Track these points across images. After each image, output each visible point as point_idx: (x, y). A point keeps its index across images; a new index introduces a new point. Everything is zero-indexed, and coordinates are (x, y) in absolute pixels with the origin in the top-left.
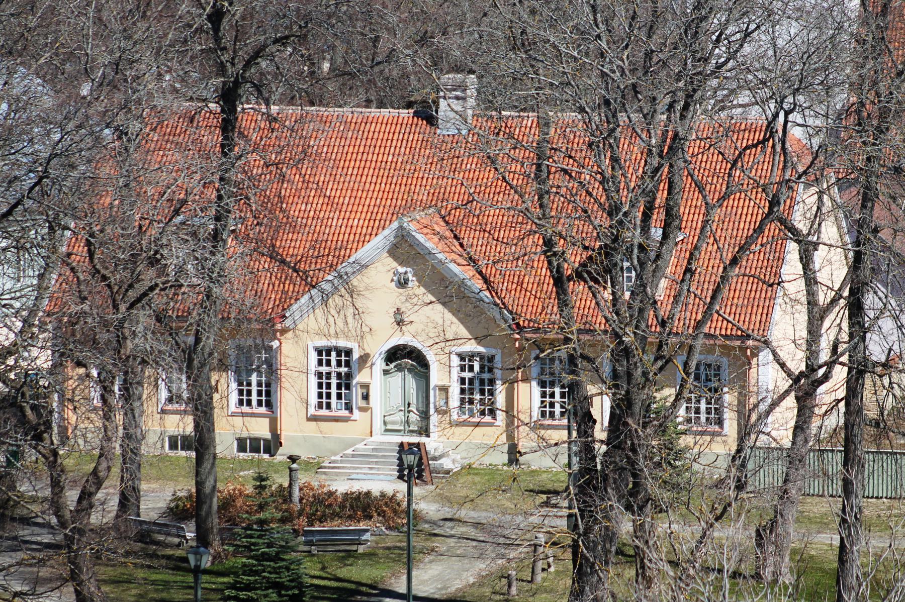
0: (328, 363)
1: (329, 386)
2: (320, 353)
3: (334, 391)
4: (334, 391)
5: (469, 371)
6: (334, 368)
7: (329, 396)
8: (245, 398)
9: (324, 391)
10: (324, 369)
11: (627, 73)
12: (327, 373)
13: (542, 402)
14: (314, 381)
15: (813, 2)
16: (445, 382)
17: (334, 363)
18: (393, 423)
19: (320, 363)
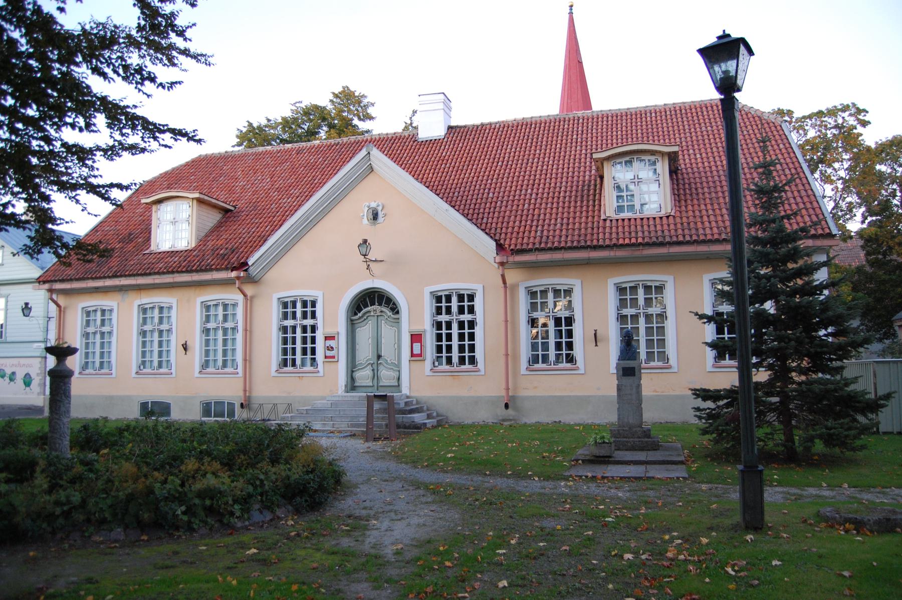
1: (449, 337)
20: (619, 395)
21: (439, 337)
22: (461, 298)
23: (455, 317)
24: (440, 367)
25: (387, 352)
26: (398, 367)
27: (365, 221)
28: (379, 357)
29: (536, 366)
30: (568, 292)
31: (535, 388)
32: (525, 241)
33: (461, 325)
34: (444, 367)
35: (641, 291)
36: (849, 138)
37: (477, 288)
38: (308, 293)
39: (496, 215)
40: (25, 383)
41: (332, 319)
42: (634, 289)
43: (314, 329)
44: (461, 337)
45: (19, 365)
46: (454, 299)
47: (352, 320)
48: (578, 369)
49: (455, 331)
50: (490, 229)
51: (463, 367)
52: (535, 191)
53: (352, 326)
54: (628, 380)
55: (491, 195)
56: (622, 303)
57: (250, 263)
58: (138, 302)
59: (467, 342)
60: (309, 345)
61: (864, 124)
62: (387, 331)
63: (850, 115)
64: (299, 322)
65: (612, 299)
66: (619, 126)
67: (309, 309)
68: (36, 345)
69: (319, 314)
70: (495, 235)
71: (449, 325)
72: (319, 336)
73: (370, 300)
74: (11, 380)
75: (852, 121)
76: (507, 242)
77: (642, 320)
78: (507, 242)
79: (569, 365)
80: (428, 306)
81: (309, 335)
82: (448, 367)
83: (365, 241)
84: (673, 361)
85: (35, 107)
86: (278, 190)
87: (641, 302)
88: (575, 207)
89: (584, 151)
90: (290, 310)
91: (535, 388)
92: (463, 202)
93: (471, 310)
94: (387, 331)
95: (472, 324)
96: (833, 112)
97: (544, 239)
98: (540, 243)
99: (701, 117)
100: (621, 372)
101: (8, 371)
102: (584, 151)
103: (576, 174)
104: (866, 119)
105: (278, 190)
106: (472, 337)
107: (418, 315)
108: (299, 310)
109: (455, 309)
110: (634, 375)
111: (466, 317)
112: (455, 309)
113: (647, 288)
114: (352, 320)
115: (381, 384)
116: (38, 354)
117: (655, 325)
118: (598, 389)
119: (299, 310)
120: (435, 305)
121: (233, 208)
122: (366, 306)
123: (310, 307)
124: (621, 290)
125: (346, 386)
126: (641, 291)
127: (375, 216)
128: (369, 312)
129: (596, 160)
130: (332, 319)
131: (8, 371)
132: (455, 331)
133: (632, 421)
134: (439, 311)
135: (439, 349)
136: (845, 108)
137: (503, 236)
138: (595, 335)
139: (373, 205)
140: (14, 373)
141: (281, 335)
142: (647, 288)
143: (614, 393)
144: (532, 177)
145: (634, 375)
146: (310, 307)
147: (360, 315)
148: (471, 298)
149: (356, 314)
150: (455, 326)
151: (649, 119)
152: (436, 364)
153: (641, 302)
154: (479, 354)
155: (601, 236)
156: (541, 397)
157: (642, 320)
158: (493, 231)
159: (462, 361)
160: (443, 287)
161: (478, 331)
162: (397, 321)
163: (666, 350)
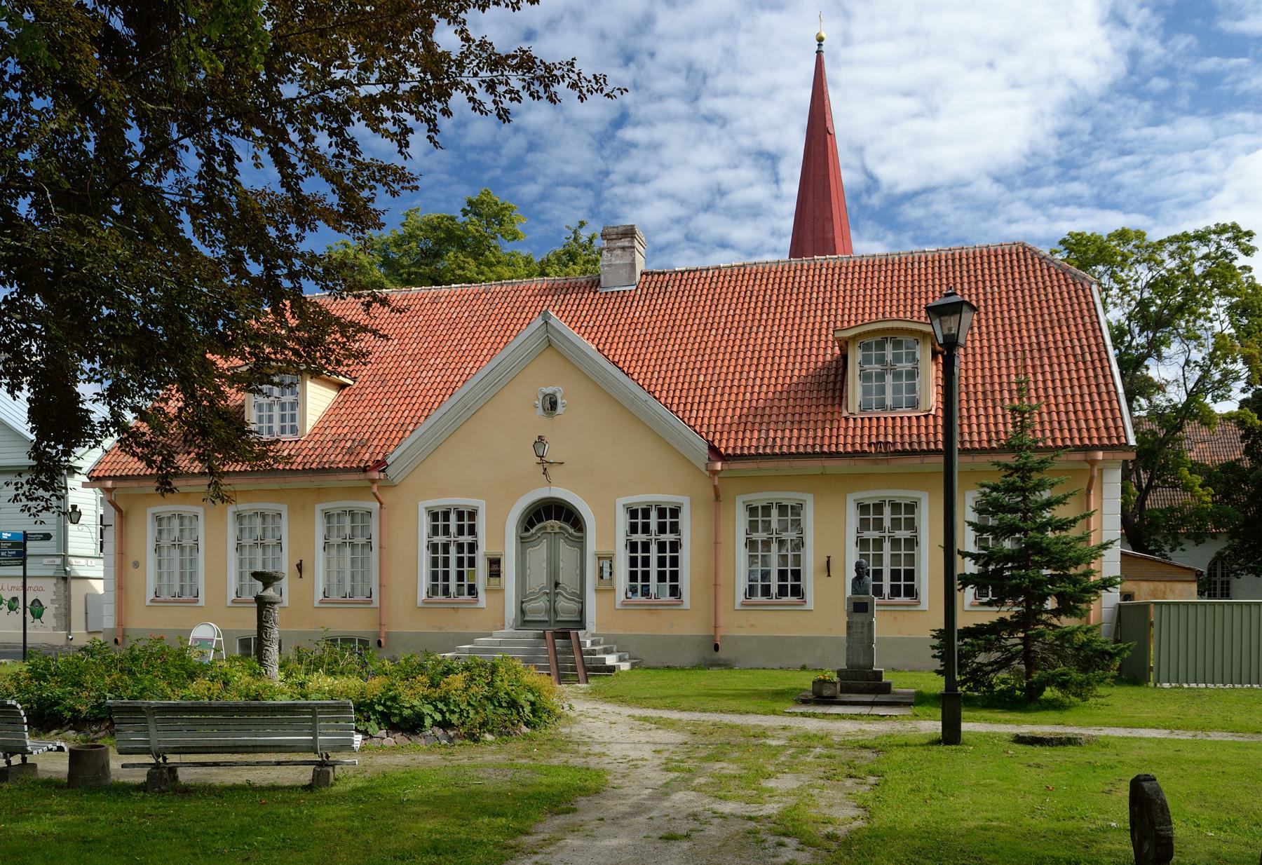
0: (446, 531)
1: (646, 562)
2: (435, 516)
3: (654, 569)
4: (654, 569)
5: (643, 532)
6: (453, 537)
7: (646, 576)
8: (440, 583)
9: (640, 569)
10: (640, 537)
11: (1210, 64)
12: (643, 543)
13: (751, 572)
14: (425, 556)
15: (3, 356)
16: (606, 549)
17: (453, 529)
18: (534, 611)
19: (435, 531)
20: (849, 634)
21: (633, 562)
22: (662, 513)
24: (634, 599)
25: (567, 578)
26: (581, 597)
27: (540, 411)
28: (557, 585)
30: (911, 508)
31: (752, 626)
32: (747, 443)
34: (440, 598)
35: (887, 510)
36: (1222, 274)
37: (684, 501)
38: (465, 502)
39: (709, 406)
42: (879, 507)
43: (473, 547)
44: (662, 561)
46: (654, 514)
49: (654, 554)
50: (701, 426)
51: (897, 599)
52: (760, 374)
54: (859, 617)
55: (702, 378)
56: (864, 524)
57: (389, 461)
59: (668, 569)
60: (440, 569)
61: (1248, 251)
62: (567, 552)
63: (1228, 239)
64: (452, 539)
65: (852, 518)
66: (876, 280)
67: (466, 523)
68: (46, 561)
70: (707, 434)
71: (446, 548)
75: (1228, 246)
76: (724, 444)
77: (887, 546)
78: (724, 444)
79: (794, 599)
80: (623, 521)
81: (466, 555)
82: (764, 599)
86: (413, 357)
87: (887, 523)
89: (826, 319)
90: (440, 523)
91: (752, 626)
92: (666, 386)
93: (472, 531)
95: (675, 546)
96: (1202, 237)
97: (770, 442)
98: (765, 447)
99: (986, 271)
101: (7, 596)
102: (826, 319)
103: (814, 351)
104: (1251, 244)
105: (413, 357)
106: (675, 562)
107: (607, 534)
109: (654, 526)
110: (866, 611)
111: (668, 537)
112: (654, 526)
113: (895, 507)
116: (51, 573)
117: (903, 552)
119: (654, 521)
121: (351, 382)
122: (540, 520)
123: (467, 517)
124: (863, 508)
125: (515, 620)
126: (887, 510)
127: (553, 405)
128: (545, 528)
129: (839, 340)
130: (499, 534)
132: (654, 554)
133: (862, 661)
135: (633, 576)
136: (1221, 230)
137: (718, 435)
138: (828, 562)
139: (549, 390)
142: (895, 507)
143: (843, 633)
144: (756, 354)
145: (866, 611)
146: (467, 517)
147: (533, 531)
148: (675, 512)
149: (527, 530)
150: (453, 549)
151: (916, 271)
152: (630, 594)
153: (887, 523)
154: (685, 583)
155: (842, 440)
157: (887, 546)
158: (705, 429)
160: (640, 499)
161: (685, 555)
162: (580, 543)
163: (915, 583)
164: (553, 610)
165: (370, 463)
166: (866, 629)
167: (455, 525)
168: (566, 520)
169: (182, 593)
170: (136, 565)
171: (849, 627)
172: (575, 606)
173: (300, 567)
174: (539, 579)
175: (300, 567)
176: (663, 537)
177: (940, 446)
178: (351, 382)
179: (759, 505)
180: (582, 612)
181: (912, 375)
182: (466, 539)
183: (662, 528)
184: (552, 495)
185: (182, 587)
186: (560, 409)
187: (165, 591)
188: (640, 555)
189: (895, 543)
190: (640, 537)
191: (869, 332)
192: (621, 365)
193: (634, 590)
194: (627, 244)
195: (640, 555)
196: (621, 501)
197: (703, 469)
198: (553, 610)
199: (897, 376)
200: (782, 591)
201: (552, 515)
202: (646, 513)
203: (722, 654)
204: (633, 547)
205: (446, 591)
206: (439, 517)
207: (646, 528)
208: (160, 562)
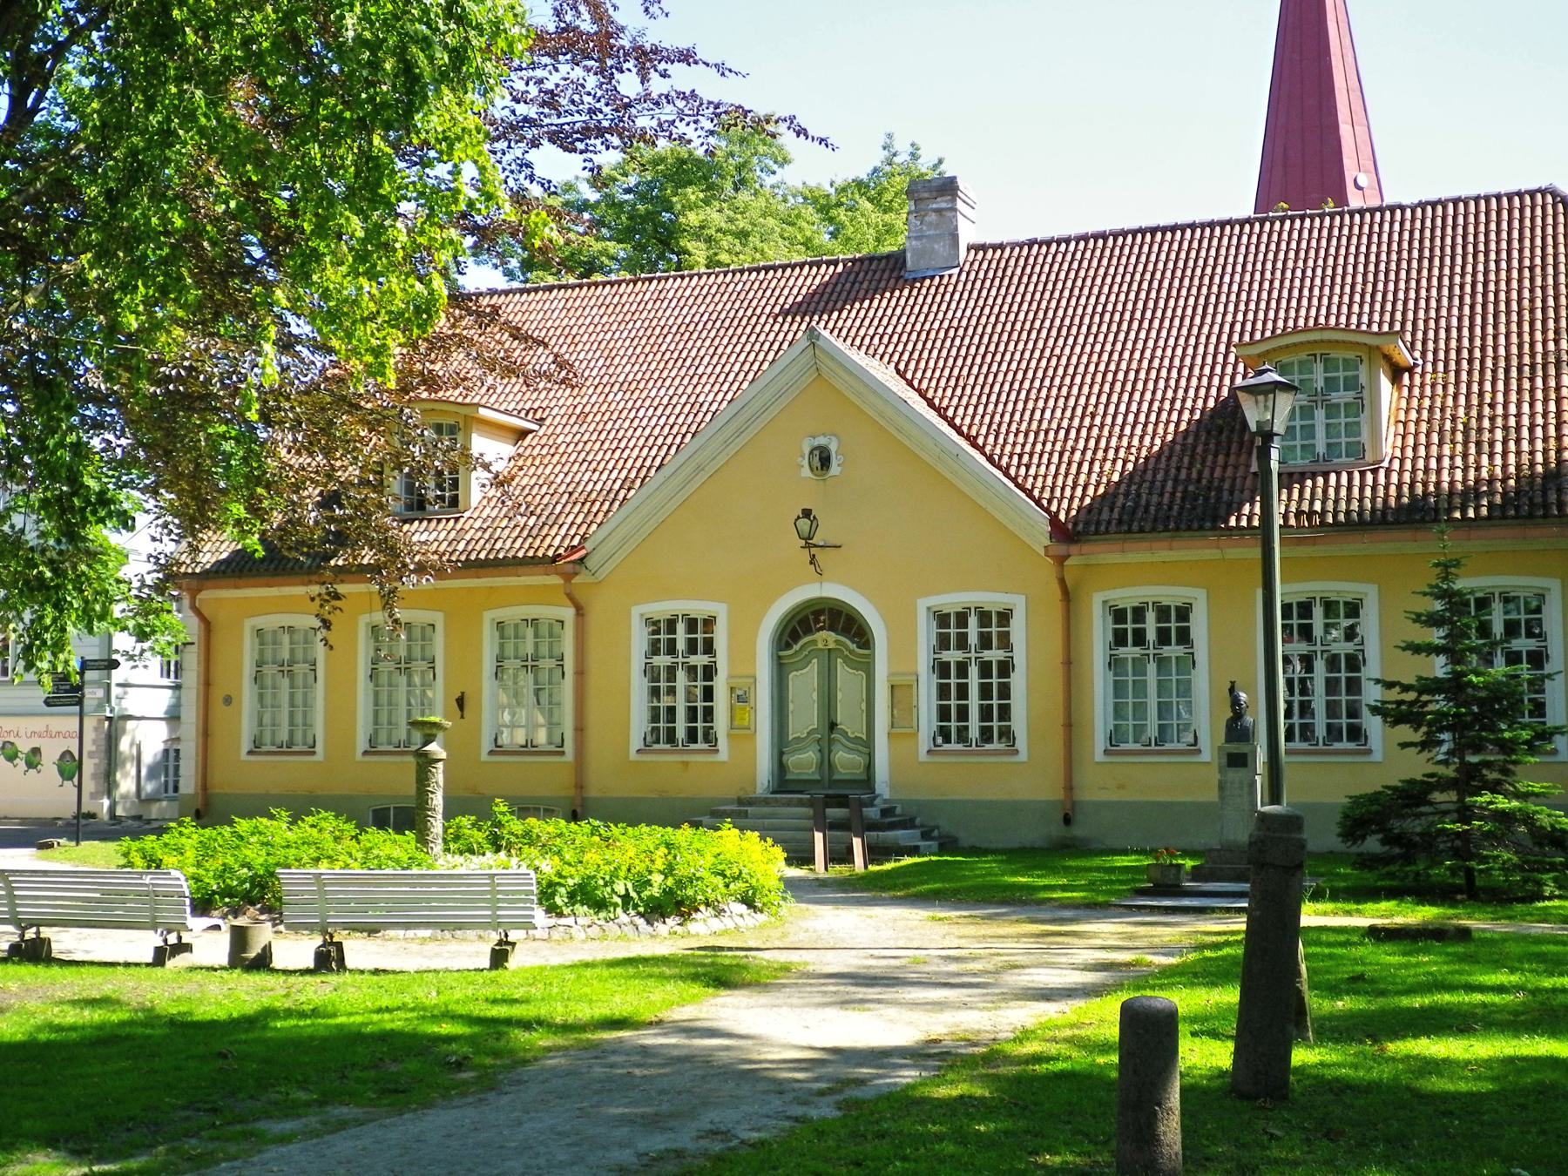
1: (963, 692)
10: (953, 656)
14: (639, 686)
21: (943, 691)
22: (692, 625)
23: (973, 655)
25: (848, 718)
26: (868, 744)
27: (806, 472)
28: (833, 726)
29: (1337, 746)
30: (1353, 609)
33: (985, 669)
38: (699, 608)
40: (61, 773)
41: (745, 655)
44: (985, 691)
45: (49, 734)
46: (1151, 616)
47: (780, 658)
48: (1369, 752)
49: (974, 680)
53: (781, 671)
54: (1236, 775)
58: (1018, 603)
59: (953, 703)
62: (847, 679)
69: (720, 644)
70: (1050, 501)
71: (962, 669)
72: (720, 685)
73: (823, 626)
74: (31, 765)
80: (925, 634)
83: (807, 513)
84: (1021, 743)
85: (260, 235)
88: (1428, 447)
93: (709, 648)
94: (847, 679)
95: (1006, 668)
100: (1224, 761)
101: (24, 746)
106: (1005, 691)
107: (903, 652)
108: (1151, 626)
111: (994, 655)
113: (1330, 607)
114: (780, 658)
115: (836, 777)
118: (1121, 787)
119: (1151, 626)
120: (1111, 626)
121: (536, 427)
123: (701, 632)
130: (745, 655)
131: (24, 746)
132: (974, 680)
134: (943, 642)
139: (821, 441)
140: (36, 751)
141: (935, 680)
146: (701, 632)
147: (796, 647)
149: (788, 646)
150: (973, 671)
152: (939, 740)
154: (1018, 723)
156: (1131, 803)
159: (986, 734)
160: (952, 601)
161: (1017, 681)
162: (868, 668)
164: (826, 763)
165: (561, 551)
166: (1246, 790)
167: (684, 642)
168: (845, 631)
169: (290, 744)
170: (228, 700)
171: (1222, 787)
172: (860, 760)
173: (461, 702)
174: (805, 718)
175: (461, 702)
176: (1167, 651)
177: (1256, 523)
178: (536, 427)
179: (952, 610)
180: (870, 767)
181: (1356, 407)
182: (700, 660)
183: (985, 642)
184: (825, 594)
185: (291, 733)
186: (835, 469)
187: (383, 737)
188: (953, 681)
189: (692, 670)
190: (953, 656)
191: (1287, 346)
192: (930, 395)
193: (945, 734)
194: (944, 205)
195: (953, 681)
196: (923, 604)
197: (1042, 552)
198: (826, 763)
199: (1332, 410)
200: (1333, 733)
201: (823, 626)
202: (962, 619)
203: (1078, 831)
204: (943, 669)
205: (963, 735)
206: (661, 632)
207: (962, 643)
208: (376, 694)
